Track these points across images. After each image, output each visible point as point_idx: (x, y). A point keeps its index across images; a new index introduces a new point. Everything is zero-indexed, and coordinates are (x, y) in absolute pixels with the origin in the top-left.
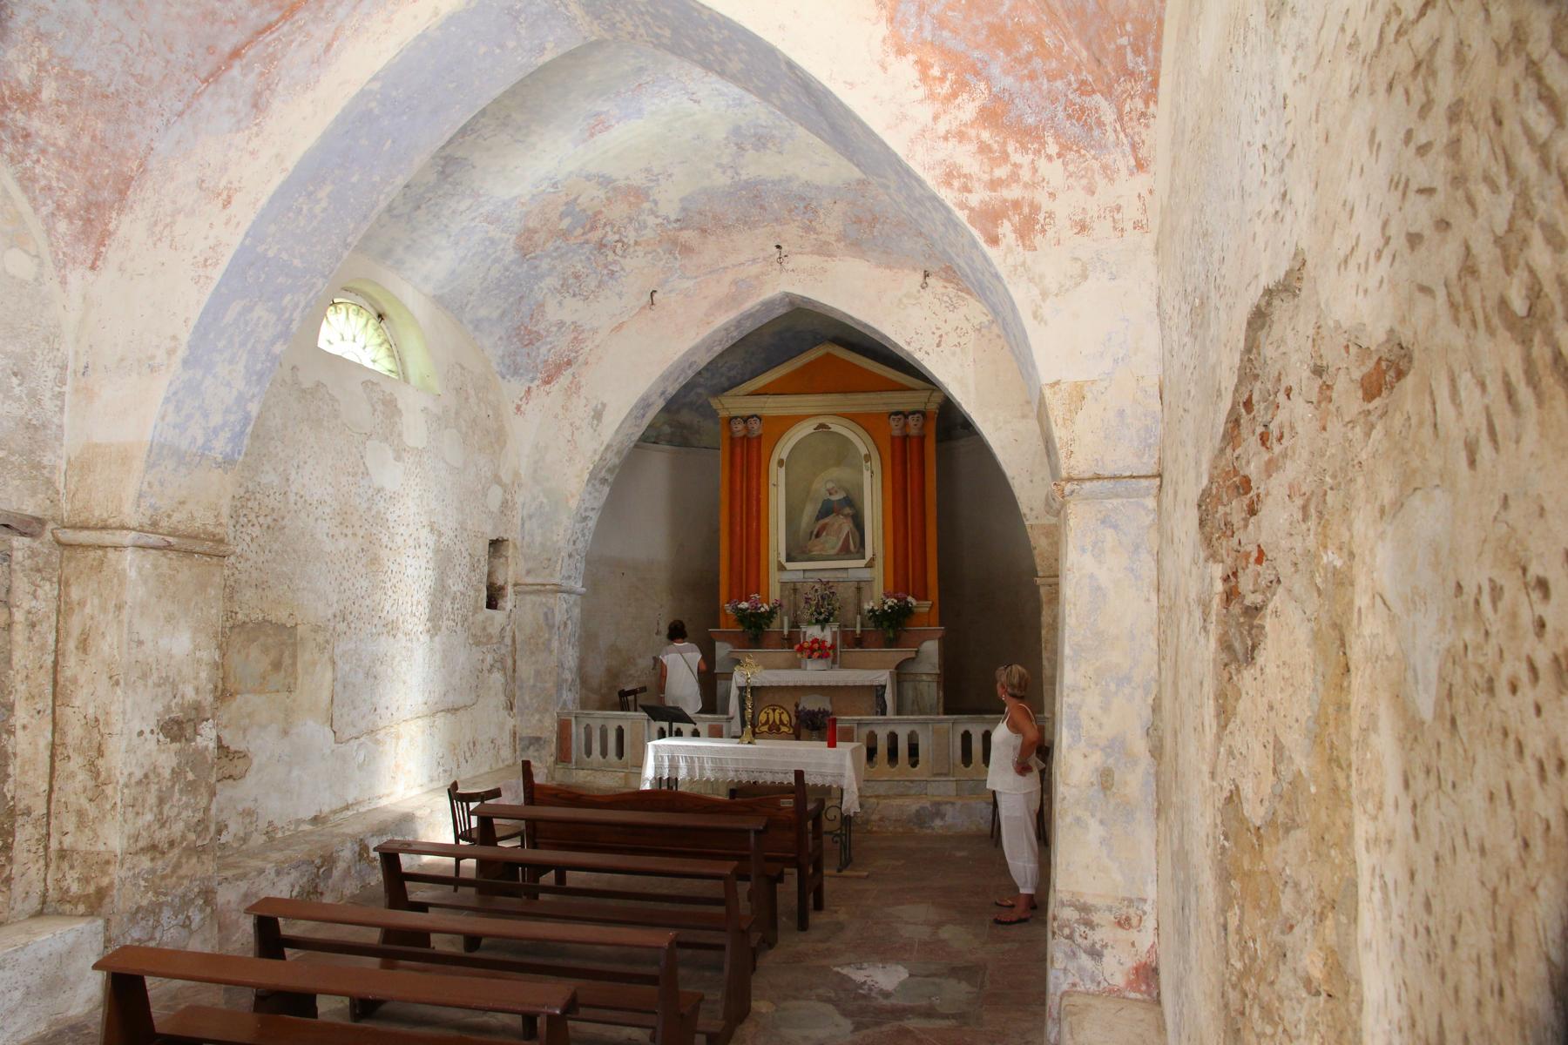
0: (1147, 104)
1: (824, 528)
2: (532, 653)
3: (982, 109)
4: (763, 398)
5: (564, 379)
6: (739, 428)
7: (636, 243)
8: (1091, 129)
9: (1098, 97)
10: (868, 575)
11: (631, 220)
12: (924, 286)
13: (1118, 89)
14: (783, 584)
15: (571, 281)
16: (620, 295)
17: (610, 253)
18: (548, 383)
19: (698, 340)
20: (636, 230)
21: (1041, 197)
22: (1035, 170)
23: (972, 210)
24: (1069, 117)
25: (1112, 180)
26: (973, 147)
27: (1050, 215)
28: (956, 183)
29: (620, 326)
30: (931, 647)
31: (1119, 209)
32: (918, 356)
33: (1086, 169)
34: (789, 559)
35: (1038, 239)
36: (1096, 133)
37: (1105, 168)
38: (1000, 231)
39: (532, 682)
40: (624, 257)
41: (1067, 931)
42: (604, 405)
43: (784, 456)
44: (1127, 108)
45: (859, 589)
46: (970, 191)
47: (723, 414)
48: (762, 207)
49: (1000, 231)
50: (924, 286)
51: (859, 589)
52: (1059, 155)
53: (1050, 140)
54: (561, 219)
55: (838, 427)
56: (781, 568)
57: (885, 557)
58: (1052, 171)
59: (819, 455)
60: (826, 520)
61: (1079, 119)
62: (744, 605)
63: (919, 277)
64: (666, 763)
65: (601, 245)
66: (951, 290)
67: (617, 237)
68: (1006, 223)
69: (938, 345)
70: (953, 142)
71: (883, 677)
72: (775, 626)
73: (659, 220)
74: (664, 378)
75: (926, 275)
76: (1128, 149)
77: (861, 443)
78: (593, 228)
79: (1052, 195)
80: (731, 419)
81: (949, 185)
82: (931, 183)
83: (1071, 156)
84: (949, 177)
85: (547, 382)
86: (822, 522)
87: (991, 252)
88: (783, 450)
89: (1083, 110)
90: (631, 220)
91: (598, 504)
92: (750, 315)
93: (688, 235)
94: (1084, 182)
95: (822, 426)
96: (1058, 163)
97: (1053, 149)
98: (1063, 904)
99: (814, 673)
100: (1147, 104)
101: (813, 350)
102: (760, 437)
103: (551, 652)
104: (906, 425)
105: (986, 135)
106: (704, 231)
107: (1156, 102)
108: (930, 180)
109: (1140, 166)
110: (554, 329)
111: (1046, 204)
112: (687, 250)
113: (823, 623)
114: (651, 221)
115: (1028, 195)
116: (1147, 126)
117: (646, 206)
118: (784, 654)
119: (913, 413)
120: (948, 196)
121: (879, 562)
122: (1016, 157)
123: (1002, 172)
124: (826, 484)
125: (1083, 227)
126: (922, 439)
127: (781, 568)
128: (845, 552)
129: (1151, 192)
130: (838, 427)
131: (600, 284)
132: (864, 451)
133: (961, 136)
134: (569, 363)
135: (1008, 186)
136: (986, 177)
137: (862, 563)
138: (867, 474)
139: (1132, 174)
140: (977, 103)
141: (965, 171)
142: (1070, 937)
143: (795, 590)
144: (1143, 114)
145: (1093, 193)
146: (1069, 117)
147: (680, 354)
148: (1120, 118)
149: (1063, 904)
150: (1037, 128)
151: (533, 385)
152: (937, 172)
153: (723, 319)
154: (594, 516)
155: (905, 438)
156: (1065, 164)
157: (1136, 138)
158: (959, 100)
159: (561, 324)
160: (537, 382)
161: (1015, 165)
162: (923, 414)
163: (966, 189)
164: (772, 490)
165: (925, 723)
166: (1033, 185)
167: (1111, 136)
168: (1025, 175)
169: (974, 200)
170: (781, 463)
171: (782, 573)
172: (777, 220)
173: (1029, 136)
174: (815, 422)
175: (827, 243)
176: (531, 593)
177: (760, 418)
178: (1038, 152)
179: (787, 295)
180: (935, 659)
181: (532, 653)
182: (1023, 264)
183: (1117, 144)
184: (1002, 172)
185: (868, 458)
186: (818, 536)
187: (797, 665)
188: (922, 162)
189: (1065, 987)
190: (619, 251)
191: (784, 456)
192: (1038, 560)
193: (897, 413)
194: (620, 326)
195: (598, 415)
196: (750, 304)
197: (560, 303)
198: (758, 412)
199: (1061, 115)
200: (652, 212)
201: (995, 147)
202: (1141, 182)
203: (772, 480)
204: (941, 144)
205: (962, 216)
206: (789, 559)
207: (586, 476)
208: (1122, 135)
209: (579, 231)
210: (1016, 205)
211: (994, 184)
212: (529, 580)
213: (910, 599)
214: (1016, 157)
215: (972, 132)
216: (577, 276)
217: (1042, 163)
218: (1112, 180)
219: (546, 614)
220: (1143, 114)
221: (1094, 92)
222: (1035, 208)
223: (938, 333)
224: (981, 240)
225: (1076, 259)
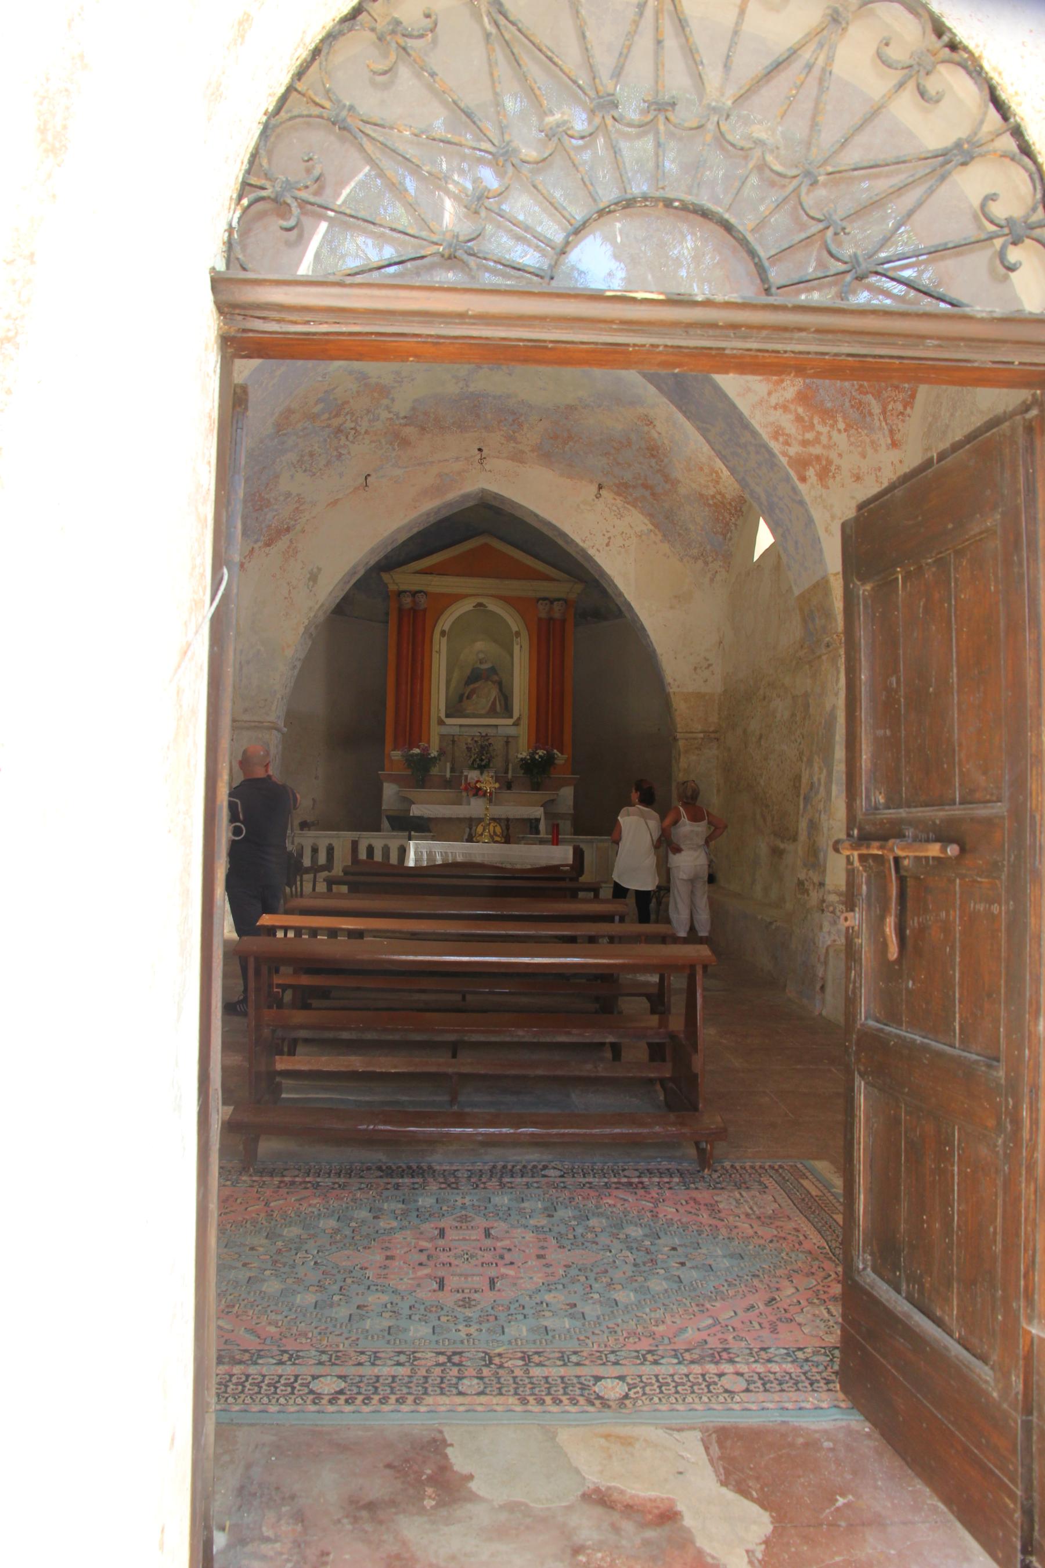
0: (905, 408)
1: (473, 692)
3: (799, 393)
4: (429, 577)
5: (282, 544)
6: (407, 601)
7: (366, 432)
8: (865, 416)
9: (870, 396)
10: (515, 730)
11: (368, 411)
12: (598, 496)
13: (885, 394)
14: (442, 737)
15: (306, 458)
16: (341, 475)
17: (343, 438)
18: (269, 545)
19: (406, 521)
20: (370, 421)
21: (833, 455)
22: (830, 438)
23: (790, 457)
24: (852, 406)
25: (876, 451)
26: (792, 417)
27: (838, 468)
28: (781, 439)
29: (336, 502)
30: (567, 793)
31: (880, 469)
32: (591, 552)
33: (861, 442)
34: (447, 716)
35: (830, 482)
36: (868, 419)
37: (872, 442)
38: (807, 474)
40: (353, 442)
41: (831, 909)
42: (319, 569)
43: (446, 628)
44: (890, 407)
45: (507, 743)
46: (789, 445)
47: (392, 587)
48: (478, 416)
49: (807, 474)
50: (598, 496)
51: (507, 743)
52: (845, 430)
53: (840, 420)
54: (316, 404)
55: (493, 606)
56: (441, 722)
57: (529, 717)
58: (841, 439)
59: (478, 631)
60: (476, 685)
61: (858, 409)
62: (416, 751)
63: (594, 489)
64: (425, 857)
65: (339, 430)
66: (619, 501)
67: (353, 425)
68: (811, 470)
69: (607, 545)
70: (780, 411)
71: (538, 812)
72: (435, 771)
73: (391, 416)
74: (372, 551)
75: (600, 487)
76: (887, 432)
77: (514, 622)
78: (337, 415)
79: (840, 455)
80: (400, 593)
81: (776, 439)
82: (765, 437)
83: (852, 431)
84: (776, 435)
85: (268, 544)
86: (472, 686)
87: (801, 486)
88: (446, 622)
89: (860, 402)
90: (368, 411)
91: (302, 657)
92: (449, 505)
93: (410, 431)
94: (860, 449)
95: (480, 605)
96: (844, 435)
97: (841, 425)
98: (829, 892)
100: (905, 408)
101: (478, 537)
102: (425, 610)
105: (800, 410)
106: (423, 429)
107: (912, 408)
108: (765, 434)
109: (894, 444)
110: (282, 498)
111: (837, 461)
112: (405, 443)
113: (482, 768)
114: (384, 415)
115: (825, 453)
116: (903, 421)
117: (385, 402)
119: (558, 600)
120: (775, 446)
121: (525, 722)
122: (819, 428)
123: (810, 436)
124: (479, 649)
125: (858, 478)
126: (563, 621)
127: (441, 722)
128: (492, 712)
129: (901, 462)
130: (493, 606)
131: (328, 464)
132: (515, 629)
133: (785, 408)
134: (288, 530)
135: (813, 445)
136: (800, 438)
137: (510, 721)
138: (516, 649)
139: (888, 449)
140: (796, 388)
141: (787, 431)
142: (833, 912)
143: (453, 741)
144: (902, 413)
145: (865, 457)
146: (852, 406)
147: (389, 532)
148: (884, 412)
149: (829, 892)
150: (832, 410)
151: (256, 546)
152: (769, 430)
153: (429, 505)
154: (299, 664)
155: (550, 619)
156: (849, 437)
157: (894, 427)
158: (784, 385)
159: (288, 495)
160: (260, 544)
161: (818, 432)
162: (565, 601)
163: (787, 443)
164: (435, 656)
165: (591, 842)
166: (827, 447)
167: (877, 424)
168: (824, 440)
169: (792, 451)
170: (443, 633)
171: (441, 725)
172: (486, 428)
173: (827, 415)
175: (522, 452)
176: (248, 729)
177: (425, 593)
178: (832, 426)
179: (483, 491)
180: (570, 802)
182: (821, 496)
183: (881, 428)
184: (810, 436)
185: (518, 634)
186: (468, 698)
187: (459, 803)
188: (758, 421)
189: (829, 943)
190: (351, 438)
191: (446, 628)
192: (678, 719)
193: (544, 599)
194: (336, 502)
195: (314, 578)
196: (451, 496)
197: (292, 476)
199: (847, 404)
200: (388, 408)
201: (806, 418)
202: (894, 455)
203: (436, 647)
204: (772, 411)
205: (784, 460)
206: (447, 716)
207: (302, 630)
208: (884, 424)
209: (326, 416)
210: (818, 458)
211: (805, 443)
212: (246, 717)
214: (819, 428)
215: (792, 407)
216: (312, 455)
217: (835, 434)
218: (876, 451)
220: (902, 413)
221: (867, 393)
222: (830, 462)
223: (608, 535)
224: (795, 478)
225: (853, 498)
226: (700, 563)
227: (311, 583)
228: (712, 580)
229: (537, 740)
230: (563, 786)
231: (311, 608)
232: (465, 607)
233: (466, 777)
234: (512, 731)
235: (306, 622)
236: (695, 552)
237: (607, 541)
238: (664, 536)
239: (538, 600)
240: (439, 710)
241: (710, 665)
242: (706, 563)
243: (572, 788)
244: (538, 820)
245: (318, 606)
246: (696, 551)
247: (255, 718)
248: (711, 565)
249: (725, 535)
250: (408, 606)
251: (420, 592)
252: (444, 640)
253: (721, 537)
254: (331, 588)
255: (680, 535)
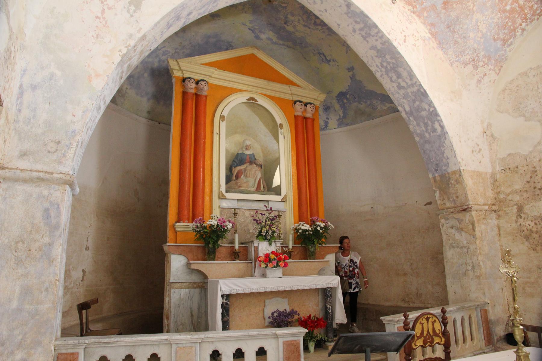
2: (19, 262)
6: (191, 87)
32: (395, 44)
39: (15, 304)
55: (262, 101)
56: (221, 197)
72: (223, 243)
77: (279, 117)
80: (184, 80)
99: (275, 280)
102: (206, 96)
103: (51, 261)
104: (305, 110)
118: (239, 265)
128: (258, 190)
137: (279, 198)
138: (281, 137)
171: (222, 203)
174: (248, 96)
176: (25, 181)
181: (19, 262)
187: (251, 274)
198: (207, 80)
207: (117, 59)
212: (23, 164)
213: (329, 223)
219: (47, 211)
226: (470, 67)
227: (133, 8)
228: (479, 82)
229: (300, 216)
230: (328, 254)
231: (131, 36)
232: (240, 98)
233: (257, 249)
234: (281, 206)
235: (124, 51)
236: (467, 58)
237: (404, 38)
238: (440, 44)
239: (295, 102)
240: (219, 186)
241: (480, 150)
242: (476, 67)
243: (334, 254)
244: (333, 289)
245: (140, 35)
246: (468, 57)
247: (39, 167)
248: (480, 69)
249: (505, 41)
250: (192, 91)
251: (204, 80)
252: (223, 124)
253: (499, 43)
254: (158, 18)
255: (456, 42)
